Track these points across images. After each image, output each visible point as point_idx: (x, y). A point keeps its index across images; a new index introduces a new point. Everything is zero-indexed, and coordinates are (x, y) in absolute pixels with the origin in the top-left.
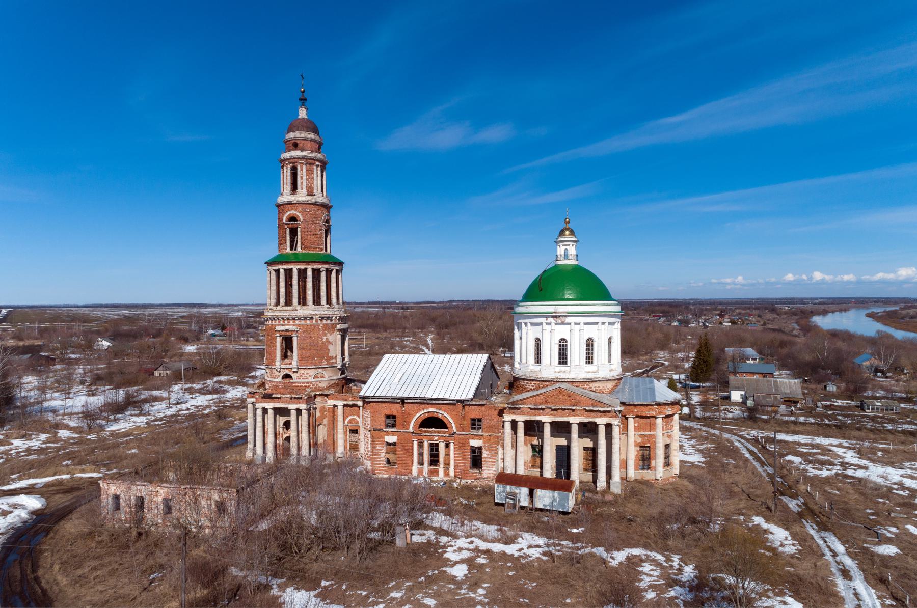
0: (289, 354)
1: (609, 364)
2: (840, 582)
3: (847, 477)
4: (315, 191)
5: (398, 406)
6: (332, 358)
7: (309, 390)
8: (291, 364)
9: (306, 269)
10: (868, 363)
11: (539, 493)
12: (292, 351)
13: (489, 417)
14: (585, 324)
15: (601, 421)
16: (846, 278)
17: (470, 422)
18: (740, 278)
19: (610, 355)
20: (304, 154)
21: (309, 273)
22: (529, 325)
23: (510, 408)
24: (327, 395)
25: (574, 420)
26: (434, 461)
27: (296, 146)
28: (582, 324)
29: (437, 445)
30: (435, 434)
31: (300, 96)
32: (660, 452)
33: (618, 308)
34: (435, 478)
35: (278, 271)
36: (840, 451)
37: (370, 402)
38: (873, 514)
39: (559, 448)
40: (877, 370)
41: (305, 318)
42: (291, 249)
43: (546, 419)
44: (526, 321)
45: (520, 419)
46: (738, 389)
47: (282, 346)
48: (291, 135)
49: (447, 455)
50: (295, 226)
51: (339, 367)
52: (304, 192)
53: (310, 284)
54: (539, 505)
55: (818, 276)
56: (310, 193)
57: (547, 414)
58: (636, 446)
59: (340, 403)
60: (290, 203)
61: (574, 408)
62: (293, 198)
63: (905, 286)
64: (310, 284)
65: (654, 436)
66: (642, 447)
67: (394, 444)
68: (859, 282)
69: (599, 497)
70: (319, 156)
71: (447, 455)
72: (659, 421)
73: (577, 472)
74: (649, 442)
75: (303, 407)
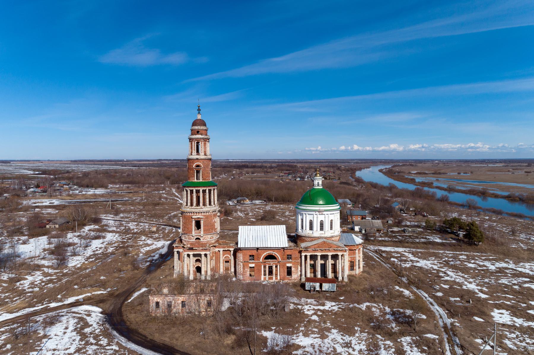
1: (337, 229)
2: (431, 307)
3: (415, 266)
10: (397, 207)
11: (324, 284)
16: (368, 148)
18: (319, 148)
21: (207, 191)
24: (215, 246)
25: (330, 254)
26: (271, 273)
29: (272, 267)
30: (271, 262)
33: (339, 207)
34: (272, 281)
36: (406, 254)
38: (430, 281)
39: (321, 264)
40: (401, 210)
42: (197, 179)
43: (319, 254)
45: (309, 254)
46: (357, 225)
49: (277, 271)
52: (203, 154)
54: (324, 289)
55: (356, 147)
59: (221, 250)
60: (197, 159)
62: (198, 157)
63: (393, 153)
64: (207, 196)
65: (355, 257)
66: (351, 262)
67: (253, 267)
68: (373, 151)
69: (340, 283)
71: (277, 271)
73: (330, 275)
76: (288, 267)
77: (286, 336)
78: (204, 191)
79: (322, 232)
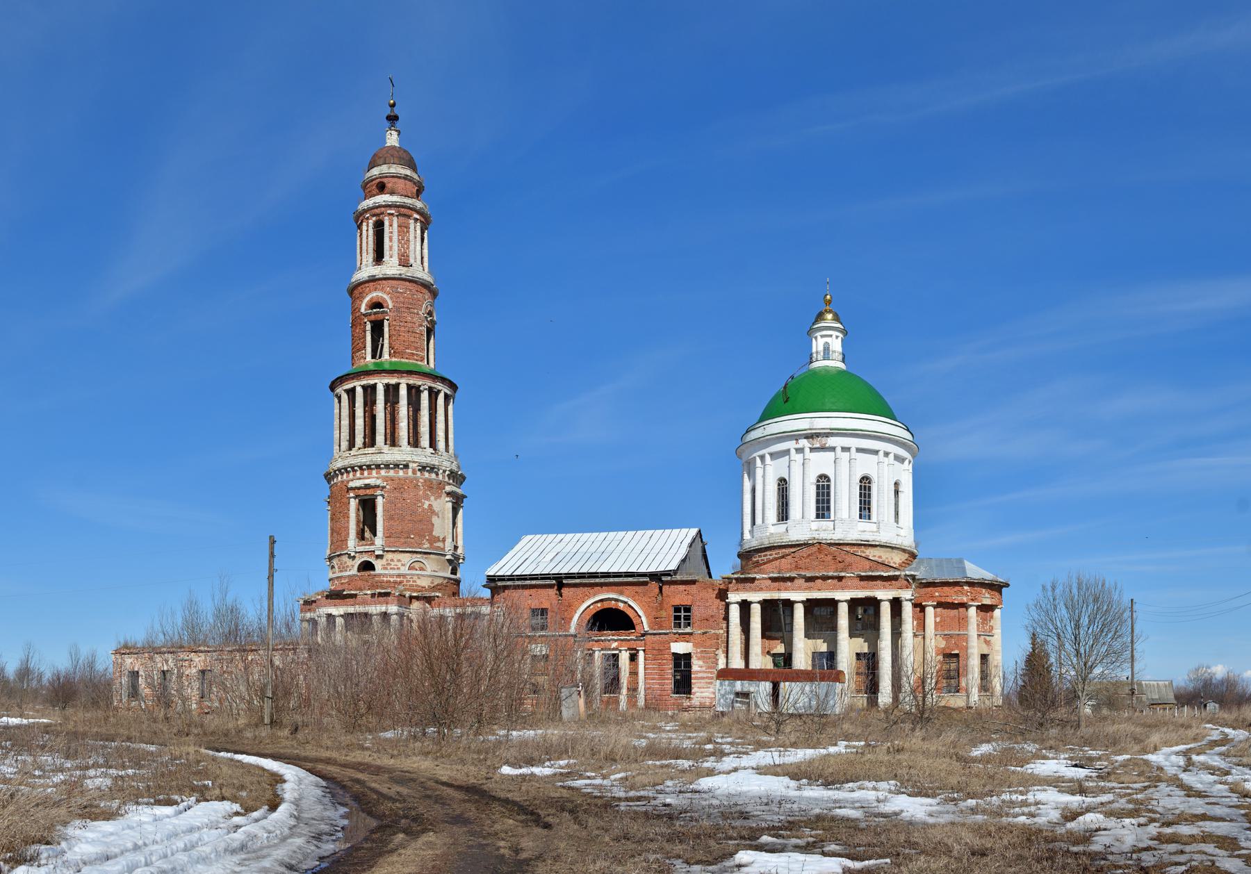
0: (368, 534)
4: (412, 261)
5: (553, 592)
6: (438, 539)
7: (401, 587)
8: (373, 544)
9: (398, 385)
11: (785, 686)
12: (374, 533)
13: (703, 603)
14: (859, 450)
15: (884, 594)
19: (897, 514)
20: (395, 199)
21: (403, 392)
22: (768, 457)
23: (736, 579)
27: (382, 188)
28: (853, 450)
30: (613, 640)
31: (388, 111)
35: (351, 393)
37: (506, 588)
41: (397, 466)
42: (374, 357)
44: (761, 453)
45: (755, 597)
47: (358, 515)
48: (375, 171)
49: (634, 673)
50: (380, 317)
51: (448, 557)
52: (395, 260)
54: (753, 666)
56: (404, 262)
57: (799, 589)
60: (373, 280)
61: (843, 574)
62: (378, 271)
65: (965, 638)
70: (419, 204)
71: (634, 673)
72: (972, 611)
74: (957, 647)
75: (393, 609)
76: (677, 658)
78: (391, 391)
79: (824, 523)
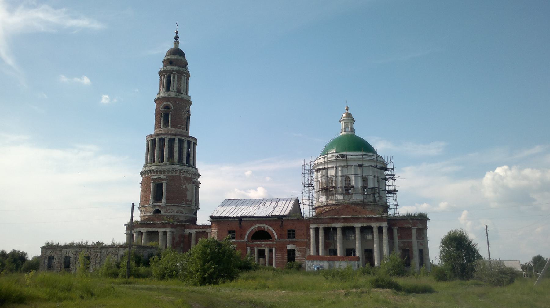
6: (189, 201)
17: (287, 232)
25: (358, 225)
30: (264, 245)
32: (416, 253)
43: (338, 225)
45: (321, 226)
53: (176, 149)
58: (400, 249)
65: (411, 242)
77: (180, 97)
